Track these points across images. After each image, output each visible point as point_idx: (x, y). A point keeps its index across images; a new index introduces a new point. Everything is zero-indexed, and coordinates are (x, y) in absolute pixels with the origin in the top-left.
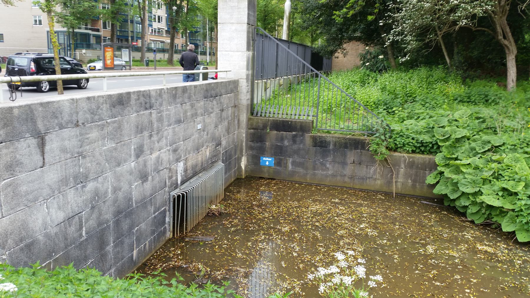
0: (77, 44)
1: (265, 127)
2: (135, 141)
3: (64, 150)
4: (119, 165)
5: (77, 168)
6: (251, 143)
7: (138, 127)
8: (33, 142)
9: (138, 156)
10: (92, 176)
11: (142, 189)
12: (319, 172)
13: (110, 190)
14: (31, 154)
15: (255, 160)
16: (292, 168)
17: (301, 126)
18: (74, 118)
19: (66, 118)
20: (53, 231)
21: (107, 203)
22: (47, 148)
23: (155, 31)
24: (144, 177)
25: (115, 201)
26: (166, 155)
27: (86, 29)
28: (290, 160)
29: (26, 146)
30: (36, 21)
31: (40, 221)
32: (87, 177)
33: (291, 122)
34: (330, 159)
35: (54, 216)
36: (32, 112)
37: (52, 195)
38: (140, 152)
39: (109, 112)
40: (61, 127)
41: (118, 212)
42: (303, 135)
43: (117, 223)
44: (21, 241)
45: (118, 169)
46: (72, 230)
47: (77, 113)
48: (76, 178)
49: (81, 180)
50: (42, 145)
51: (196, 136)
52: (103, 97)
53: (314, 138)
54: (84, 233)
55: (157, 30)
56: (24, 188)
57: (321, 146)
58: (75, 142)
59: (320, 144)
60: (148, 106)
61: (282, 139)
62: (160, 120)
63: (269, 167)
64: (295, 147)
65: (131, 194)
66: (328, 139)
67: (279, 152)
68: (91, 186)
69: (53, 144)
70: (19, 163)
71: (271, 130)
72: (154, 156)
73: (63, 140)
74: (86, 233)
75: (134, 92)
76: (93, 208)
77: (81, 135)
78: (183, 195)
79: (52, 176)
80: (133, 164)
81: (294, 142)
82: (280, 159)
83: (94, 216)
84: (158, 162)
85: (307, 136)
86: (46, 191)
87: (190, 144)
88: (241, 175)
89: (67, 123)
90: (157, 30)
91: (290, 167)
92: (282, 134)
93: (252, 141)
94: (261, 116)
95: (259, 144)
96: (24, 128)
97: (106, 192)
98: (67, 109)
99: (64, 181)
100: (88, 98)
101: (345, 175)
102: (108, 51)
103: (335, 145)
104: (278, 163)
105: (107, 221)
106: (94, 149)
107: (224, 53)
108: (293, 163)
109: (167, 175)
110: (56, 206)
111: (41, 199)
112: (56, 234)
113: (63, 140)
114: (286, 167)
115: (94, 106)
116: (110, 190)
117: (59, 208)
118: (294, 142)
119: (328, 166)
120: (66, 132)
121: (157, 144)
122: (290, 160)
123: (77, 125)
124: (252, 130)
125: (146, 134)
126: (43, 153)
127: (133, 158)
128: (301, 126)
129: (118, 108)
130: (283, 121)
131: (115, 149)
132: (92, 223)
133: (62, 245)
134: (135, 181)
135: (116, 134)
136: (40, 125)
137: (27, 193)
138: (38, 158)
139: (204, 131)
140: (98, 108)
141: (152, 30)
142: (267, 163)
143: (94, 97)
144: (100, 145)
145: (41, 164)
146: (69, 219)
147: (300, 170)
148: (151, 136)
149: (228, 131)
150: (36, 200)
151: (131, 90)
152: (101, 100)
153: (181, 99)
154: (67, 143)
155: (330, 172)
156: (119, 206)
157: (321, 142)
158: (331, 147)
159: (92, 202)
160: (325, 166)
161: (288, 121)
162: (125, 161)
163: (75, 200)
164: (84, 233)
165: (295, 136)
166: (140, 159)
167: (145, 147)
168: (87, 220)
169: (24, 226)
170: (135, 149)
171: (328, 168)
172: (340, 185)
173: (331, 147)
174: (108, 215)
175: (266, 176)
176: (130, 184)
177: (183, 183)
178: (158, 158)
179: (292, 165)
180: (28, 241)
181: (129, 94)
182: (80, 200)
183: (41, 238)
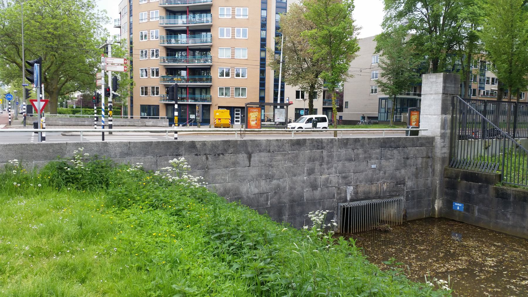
0: (403, 108)
1: (457, 177)
2: (308, 166)
3: (261, 162)
4: (295, 176)
5: (268, 172)
6: (446, 189)
7: (310, 158)
8: (245, 156)
9: (309, 174)
10: (276, 177)
11: (312, 194)
12: (501, 221)
13: (287, 188)
14: (244, 160)
15: (449, 204)
16: (478, 215)
17: (486, 178)
18: (268, 148)
19: (263, 147)
20: (252, 196)
21: (285, 194)
22: (252, 159)
23: (487, 93)
24: (314, 187)
25: (291, 194)
26: (334, 179)
27: (415, 95)
28: (476, 208)
29: (242, 157)
30: (372, 90)
31: (245, 190)
32: (273, 177)
33: (478, 174)
34: (510, 210)
35: (253, 190)
36: (246, 143)
37: (253, 180)
38: (311, 172)
39: (290, 148)
40: (260, 151)
41: (292, 201)
42: (487, 187)
43: (292, 207)
44: (236, 195)
45: (294, 178)
46: (262, 199)
47: (270, 146)
48: (266, 176)
49: (270, 178)
50: (250, 158)
51: (370, 172)
52: (286, 140)
53: (497, 190)
54: (269, 204)
55: (490, 92)
56: (239, 174)
57: (502, 198)
58: (267, 159)
59: (502, 196)
60: (320, 147)
61: (470, 188)
62: (330, 156)
63: (460, 211)
64: (481, 196)
65: (303, 193)
66: (509, 192)
67: (467, 200)
68: (275, 182)
69: (255, 158)
70: (238, 163)
71: (461, 179)
72: (323, 177)
73: (261, 157)
74: (270, 204)
75: (309, 139)
76: (275, 193)
77: (271, 156)
78: (350, 208)
79: (253, 172)
80: (305, 178)
81: (480, 191)
82: (468, 205)
83: (276, 197)
84: (327, 181)
85: (491, 187)
86: (250, 178)
87: (363, 177)
88: (435, 215)
89: (264, 150)
90: (490, 92)
91: (476, 213)
92: (471, 184)
93: (447, 188)
94: (458, 168)
95: (452, 191)
96: (242, 149)
97: (285, 188)
98: (264, 144)
99: (260, 176)
100: (277, 140)
101: (524, 227)
102: (413, 115)
103: (515, 198)
104: (467, 209)
105: (285, 203)
106: (279, 165)
107: (425, 116)
108: (479, 211)
109: (335, 192)
110: (254, 185)
111: (247, 180)
112: (253, 198)
113: (261, 157)
114: (473, 213)
115: (280, 144)
116: (287, 188)
117: (256, 187)
118: (480, 191)
119: (509, 216)
120: (263, 154)
121: (326, 170)
122: (476, 208)
123: (269, 152)
124: (447, 179)
125: (317, 163)
126: (250, 161)
127: (305, 174)
128: (486, 178)
129: (297, 147)
130: (471, 173)
131: (293, 167)
132: (275, 200)
133: (256, 204)
134: (307, 187)
135: (294, 159)
136: (250, 149)
137: (240, 176)
138: (247, 163)
139: (380, 170)
140: (283, 145)
141: (484, 92)
142: (458, 208)
143: (281, 140)
144: (282, 163)
145: (248, 165)
146: (261, 194)
147: (485, 217)
148: (321, 165)
149: (416, 176)
150: (244, 180)
151: (307, 138)
152: (285, 141)
153: (352, 146)
154: (263, 159)
155: (510, 223)
156: (293, 198)
157: (503, 194)
158: (512, 199)
159: (275, 190)
160: (506, 216)
161: (475, 173)
162: (300, 175)
163: (264, 185)
164: (269, 204)
165: (480, 187)
166: (312, 176)
167: (316, 170)
168: (271, 198)
169: (238, 189)
170: (307, 170)
171: (509, 219)
172: (519, 236)
173: (512, 199)
174: (286, 199)
175: (457, 219)
176: (303, 188)
177: (352, 200)
178: (327, 179)
179: (478, 212)
180: (239, 196)
181: (305, 140)
182: (268, 187)
183: (245, 197)
